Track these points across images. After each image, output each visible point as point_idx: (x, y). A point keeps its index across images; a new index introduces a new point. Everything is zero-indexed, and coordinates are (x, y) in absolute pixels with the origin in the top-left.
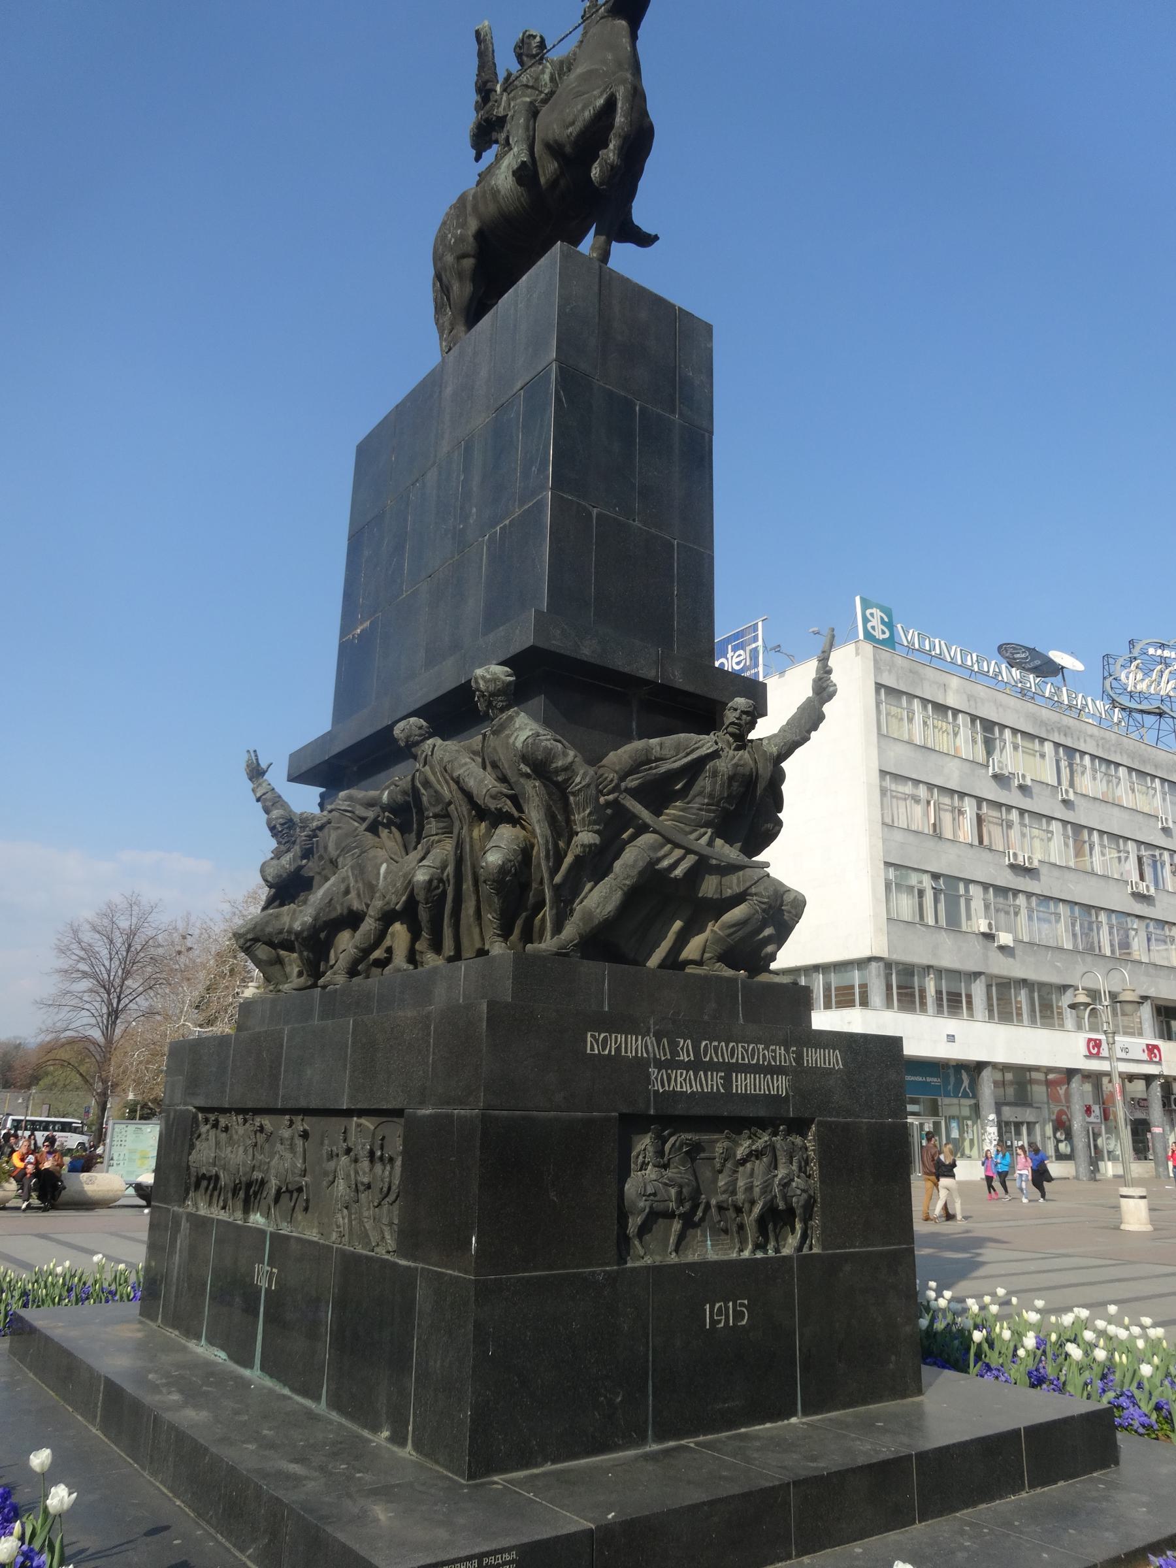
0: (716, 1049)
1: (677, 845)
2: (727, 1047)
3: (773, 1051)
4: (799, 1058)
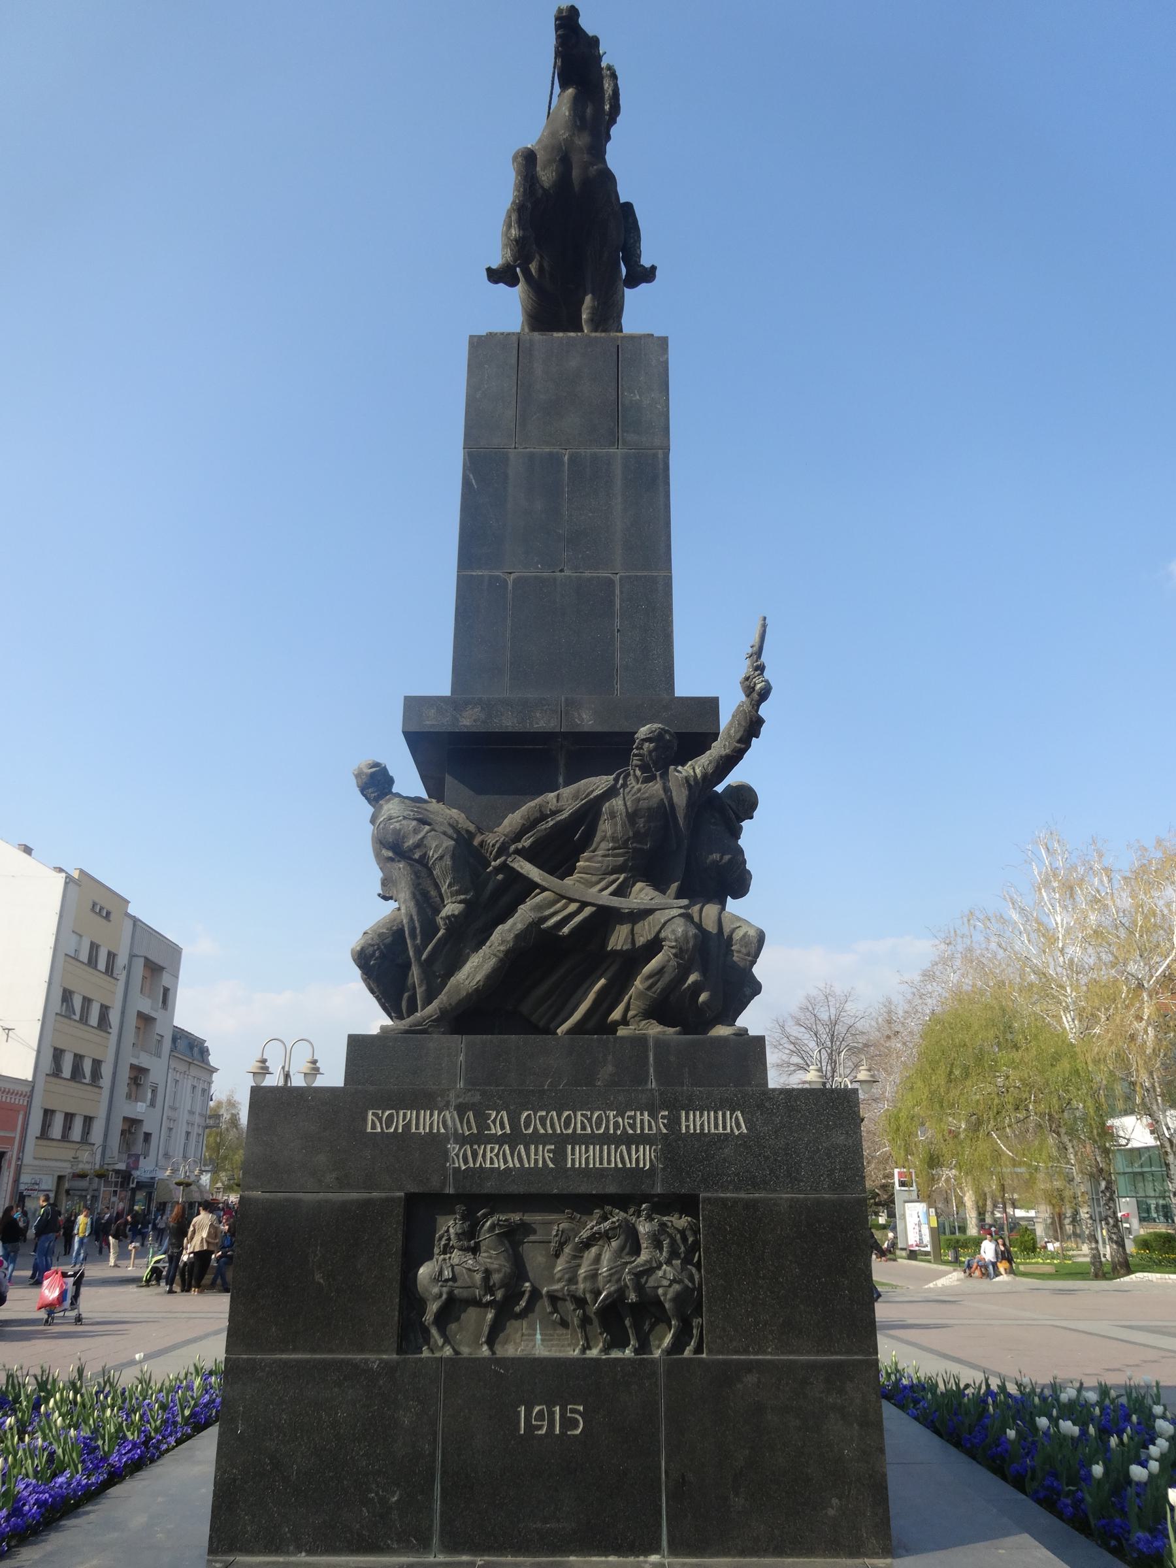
0: (543, 1120)
3: (629, 1117)
4: (674, 1122)
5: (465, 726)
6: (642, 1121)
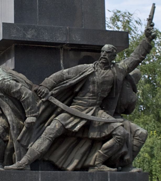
1: (76, 117)
5: (29, 38)
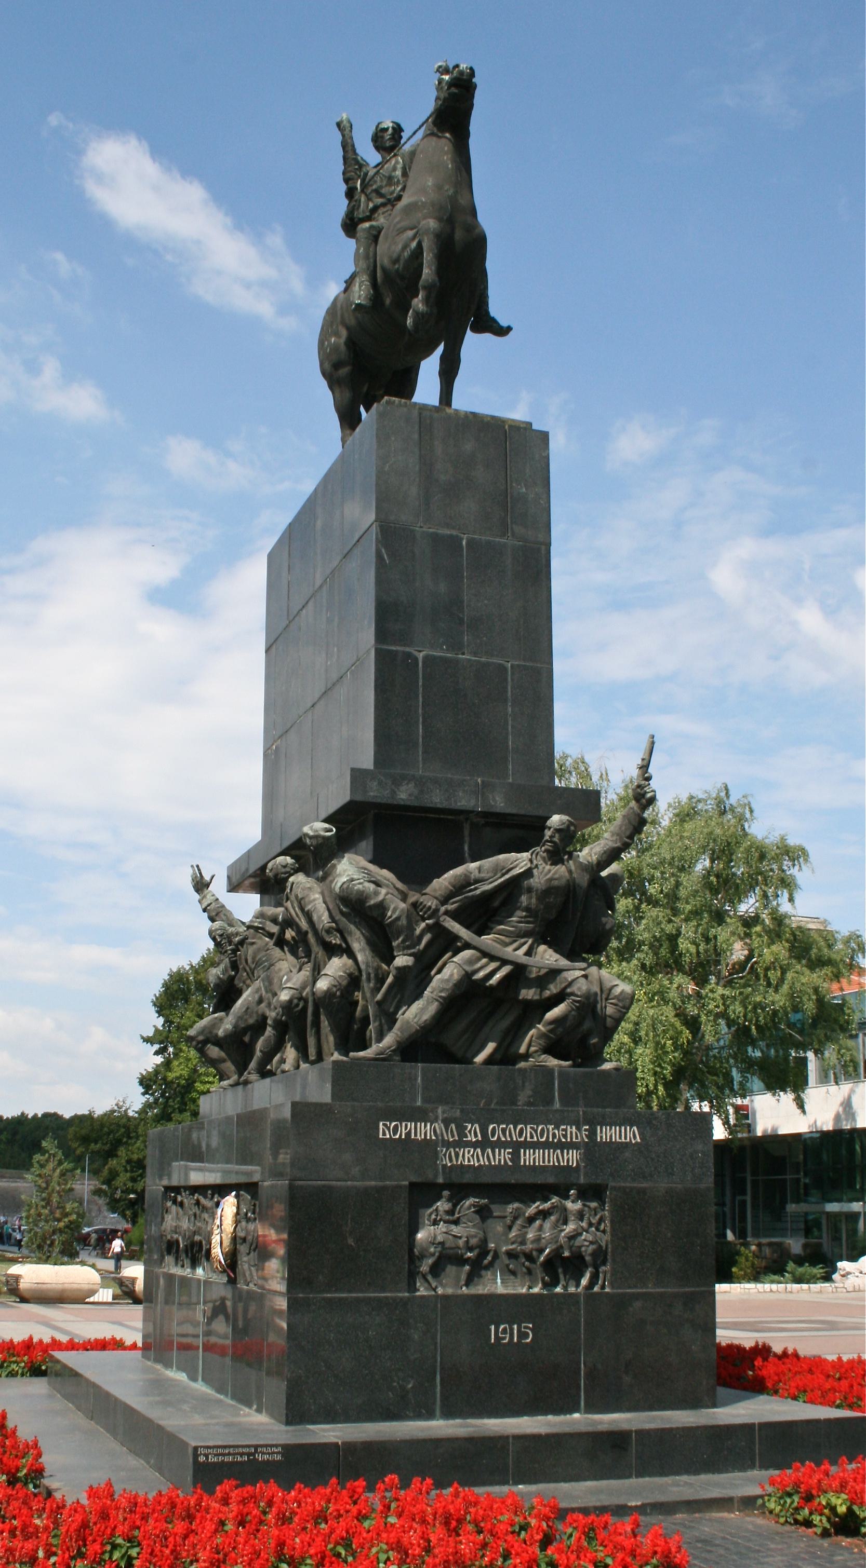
0: (504, 1131)
1: (493, 958)
2: (515, 1129)
3: (563, 1130)
4: (592, 1134)
5: (403, 800)
6: (571, 1133)
